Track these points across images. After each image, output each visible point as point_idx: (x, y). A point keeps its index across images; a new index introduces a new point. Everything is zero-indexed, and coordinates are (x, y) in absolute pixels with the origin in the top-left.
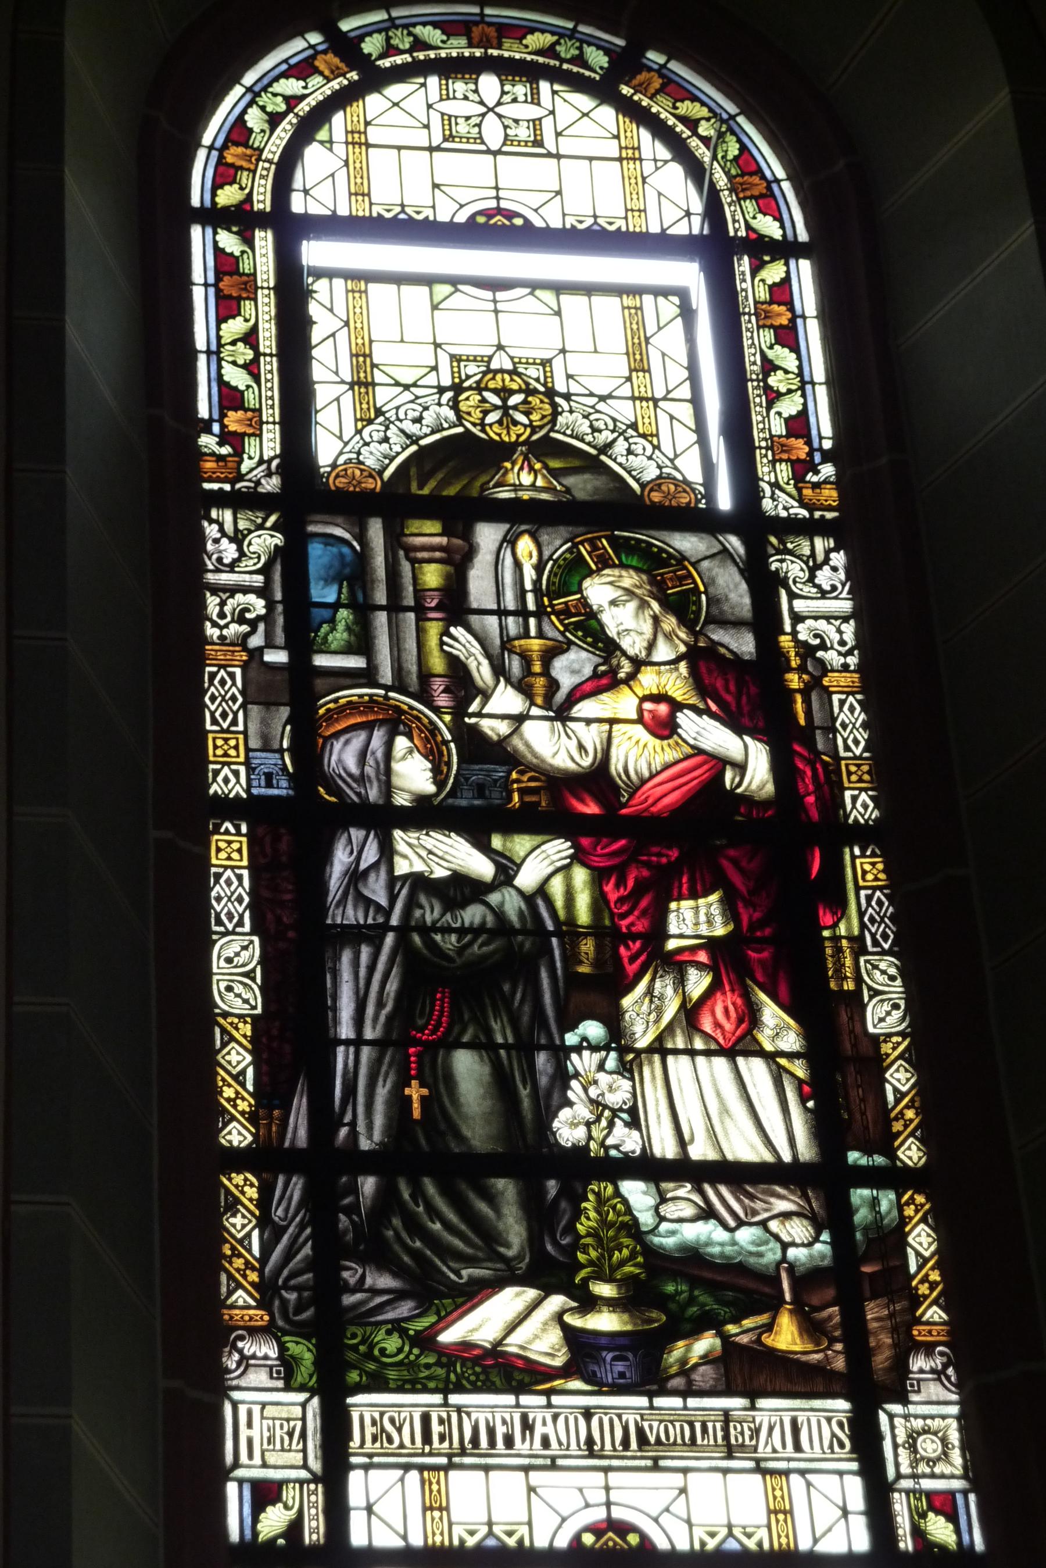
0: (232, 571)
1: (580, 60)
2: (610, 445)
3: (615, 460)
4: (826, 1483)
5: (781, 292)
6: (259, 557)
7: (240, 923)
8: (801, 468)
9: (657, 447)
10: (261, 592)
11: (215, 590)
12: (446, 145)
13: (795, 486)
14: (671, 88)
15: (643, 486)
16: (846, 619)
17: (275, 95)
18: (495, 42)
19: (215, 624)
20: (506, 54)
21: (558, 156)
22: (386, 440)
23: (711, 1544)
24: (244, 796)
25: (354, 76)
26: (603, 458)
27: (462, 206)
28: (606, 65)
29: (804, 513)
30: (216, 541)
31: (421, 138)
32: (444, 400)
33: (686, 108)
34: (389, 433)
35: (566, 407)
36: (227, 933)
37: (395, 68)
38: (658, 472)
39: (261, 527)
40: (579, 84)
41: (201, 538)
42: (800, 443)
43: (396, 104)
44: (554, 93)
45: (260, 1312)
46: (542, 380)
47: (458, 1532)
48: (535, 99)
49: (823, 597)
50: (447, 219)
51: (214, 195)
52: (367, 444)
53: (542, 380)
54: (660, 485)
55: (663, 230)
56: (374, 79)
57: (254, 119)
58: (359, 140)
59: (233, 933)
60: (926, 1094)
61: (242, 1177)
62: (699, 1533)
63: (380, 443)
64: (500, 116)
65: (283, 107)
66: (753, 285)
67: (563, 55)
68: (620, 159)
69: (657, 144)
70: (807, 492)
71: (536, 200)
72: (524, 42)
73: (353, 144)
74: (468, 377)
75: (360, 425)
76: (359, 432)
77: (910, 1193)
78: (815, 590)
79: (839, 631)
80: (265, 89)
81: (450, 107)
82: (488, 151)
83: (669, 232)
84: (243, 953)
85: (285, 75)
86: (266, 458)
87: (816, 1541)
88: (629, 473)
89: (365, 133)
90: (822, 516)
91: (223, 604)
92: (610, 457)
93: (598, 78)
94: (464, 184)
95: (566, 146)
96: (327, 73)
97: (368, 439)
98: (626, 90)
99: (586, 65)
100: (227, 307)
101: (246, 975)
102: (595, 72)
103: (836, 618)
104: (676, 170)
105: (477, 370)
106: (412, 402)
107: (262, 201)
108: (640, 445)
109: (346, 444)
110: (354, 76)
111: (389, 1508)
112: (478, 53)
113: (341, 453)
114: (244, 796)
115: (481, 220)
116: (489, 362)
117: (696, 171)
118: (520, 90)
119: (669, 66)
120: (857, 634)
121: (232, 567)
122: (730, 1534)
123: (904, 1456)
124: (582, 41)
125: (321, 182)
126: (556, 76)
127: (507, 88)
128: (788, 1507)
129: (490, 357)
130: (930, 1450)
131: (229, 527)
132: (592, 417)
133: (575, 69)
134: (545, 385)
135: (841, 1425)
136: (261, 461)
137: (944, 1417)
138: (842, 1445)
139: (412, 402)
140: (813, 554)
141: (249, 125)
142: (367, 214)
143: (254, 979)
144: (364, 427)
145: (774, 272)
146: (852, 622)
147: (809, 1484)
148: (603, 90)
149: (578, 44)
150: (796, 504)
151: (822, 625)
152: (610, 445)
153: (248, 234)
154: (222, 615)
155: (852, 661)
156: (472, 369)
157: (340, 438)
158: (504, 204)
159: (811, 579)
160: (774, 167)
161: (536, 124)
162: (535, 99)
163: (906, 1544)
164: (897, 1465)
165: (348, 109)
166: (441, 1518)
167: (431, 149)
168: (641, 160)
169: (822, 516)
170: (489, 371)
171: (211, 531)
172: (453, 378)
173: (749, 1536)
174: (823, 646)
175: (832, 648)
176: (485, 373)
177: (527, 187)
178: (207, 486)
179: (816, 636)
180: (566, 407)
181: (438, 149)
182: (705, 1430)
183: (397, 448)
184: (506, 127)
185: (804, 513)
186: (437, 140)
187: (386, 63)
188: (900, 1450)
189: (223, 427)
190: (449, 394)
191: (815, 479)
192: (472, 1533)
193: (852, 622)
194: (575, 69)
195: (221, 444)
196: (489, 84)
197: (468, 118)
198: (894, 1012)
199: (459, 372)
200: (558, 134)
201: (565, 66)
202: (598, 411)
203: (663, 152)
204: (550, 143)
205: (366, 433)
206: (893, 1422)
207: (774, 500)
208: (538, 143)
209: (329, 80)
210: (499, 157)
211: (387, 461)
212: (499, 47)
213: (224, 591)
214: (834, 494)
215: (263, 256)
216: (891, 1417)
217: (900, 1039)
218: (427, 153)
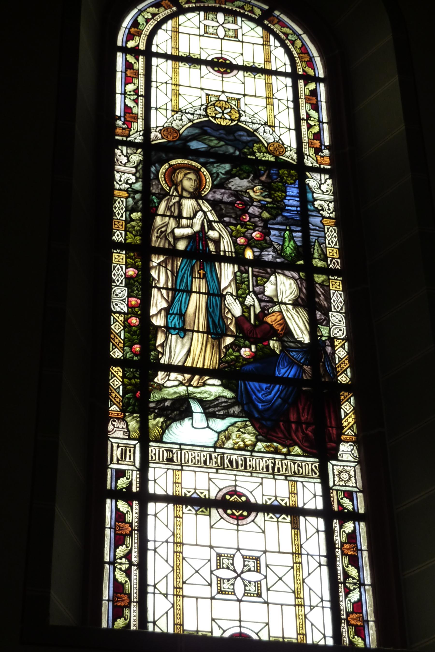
0: (125, 166)
1: (252, 11)
2: (258, 129)
3: (259, 134)
4: (310, 486)
5: (314, 93)
6: (135, 163)
7: (121, 283)
8: (318, 151)
9: (274, 131)
10: (134, 174)
11: (118, 172)
12: (205, 35)
13: (315, 156)
14: (281, 23)
15: (268, 144)
16: (331, 202)
17: (148, 13)
18: (224, 3)
19: (117, 183)
20: (227, 7)
21: (242, 42)
22: (181, 120)
23: (269, 502)
24: (123, 242)
25: (174, 9)
26: (255, 133)
27: (209, 55)
28: (261, 14)
29: (318, 165)
30: (120, 156)
31: (197, 32)
32: (202, 109)
33: (285, 30)
34: (183, 118)
35: (244, 114)
36: (117, 286)
37: (189, 8)
38: (273, 140)
39: (135, 153)
40: (250, 19)
41: (114, 154)
42: (318, 142)
43: (189, 19)
44: (242, 21)
45: (120, 413)
46: (237, 105)
47: (184, 491)
48: (235, 22)
49: (323, 194)
50: (204, 59)
51: (126, 43)
52: (175, 120)
53: (237, 105)
54: (274, 144)
55: (277, 69)
56: (182, 11)
57: (140, 20)
58: (176, 31)
59: (119, 286)
60: (352, 355)
61: (117, 368)
62: (265, 498)
63: (179, 120)
64: (223, 27)
65: (150, 17)
66: (304, 90)
67: (246, 9)
68: (263, 45)
69: (276, 41)
70: (319, 158)
71: (234, 56)
72: (234, 4)
73: (174, 31)
74: (211, 101)
75: (173, 113)
76: (173, 116)
77: (343, 392)
78: (321, 191)
79: (328, 205)
80: (145, 10)
81: (207, 22)
82: (219, 38)
83: (278, 70)
84: (122, 293)
85: (152, 6)
86: (139, 130)
87: (304, 504)
88: (264, 139)
89: (178, 28)
90: (324, 167)
91: (121, 177)
92: (258, 133)
93: (257, 17)
94: (210, 49)
95: (245, 39)
96: (166, 7)
97: (175, 119)
98: (266, 22)
99: (254, 13)
100: (127, 81)
101: (122, 300)
102: (256, 15)
103: (327, 201)
104: (282, 50)
105: (214, 99)
106: (191, 108)
107: (142, 47)
108: (268, 129)
109: (168, 119)
110: (174, 9)
111: (161, 481)
112: (218, 5)
113: (166, 122)
114: (123, 242)
115: (215, 60)
116: (219, 97)
117: (288, 52)
118: (231, 19)
119: (280, 16)
120: (335, 207)
121: (125, 165)
122: (276, 500)
123: (337, 478)
124: (253, 6)
125: (162, 42)
126: (243, 16)
127: (226, 18)
128: (296, 492)
129: (220, 96)
130: (345, 478)
131: (125, 152)
132: (252, 119)
133: (250, 14)
134: (237, 107)
135: (316, 467)
136: (137, 131)
137: (339, 485)
138: (315, 473)
139: (191, 108)
140: (321, 180)
141: (139, 21)
142: (178, 54)
143: (125, 302)
144: (174, 114)
145: (312, 86)
146: (333, 203)
147: (304, 486)
148: (259, 22)
149: (252, 6)
150: (315, 162)
151: (323, 203)
152: (258, 129)
153: (137, 57)
154: (120, 181)
155: (333, 215)
156: (213, 99)
157: (166, 117)
158: (224, 56)
159: (320, 188)
160: (314, 52)
161: (236, 31)
162: (235, 22)
163: (336, 508)
164: (334, 481)
165: (173, 20)
166: (179, 486)
167: (200, 36)
168: (270, 46)
169: (324, 167)
170: (219, 100)
171: (118, 152)
172: (206, 101)
173: (282, 500)
174: (322, 210)
175: (325, 211)
176: (217, 101)
177: (232, 52)
178: (117, 138)
179: (320, 206)
180: (244, 114)
181: (203, 36)
182: (267, 467)
183: (185, 123)
184: (225, 31)
185: (318, 165)
186: (202, 33)
187: (187, 6)
188: (336, 476)
189: (125, 119)
190: (204, 107)
191: (322, 155)
192: (189, 492)
193: (333, 203)
194: (250, 14)
195: (123, 124)
196: (221, 17)
197: (213, 27)
198: (340, 332)
199: (208, 99)
200: (243, 35)
201: (246, 13)
202: (254, 117)
203: (278, 44)
204: (240, 38)
205: (175, 117)
206: (333, 467)
207: (307, 160)
208: (236, 37)
209: (166, 9)
210: (223, 41)
211: (181, 127)
212: (225, 4)
213: (122, 172)
214: (328, 160)
215: (140, 65)
216: (333, 465)
217: (341, 341)
218: (199, 37)
